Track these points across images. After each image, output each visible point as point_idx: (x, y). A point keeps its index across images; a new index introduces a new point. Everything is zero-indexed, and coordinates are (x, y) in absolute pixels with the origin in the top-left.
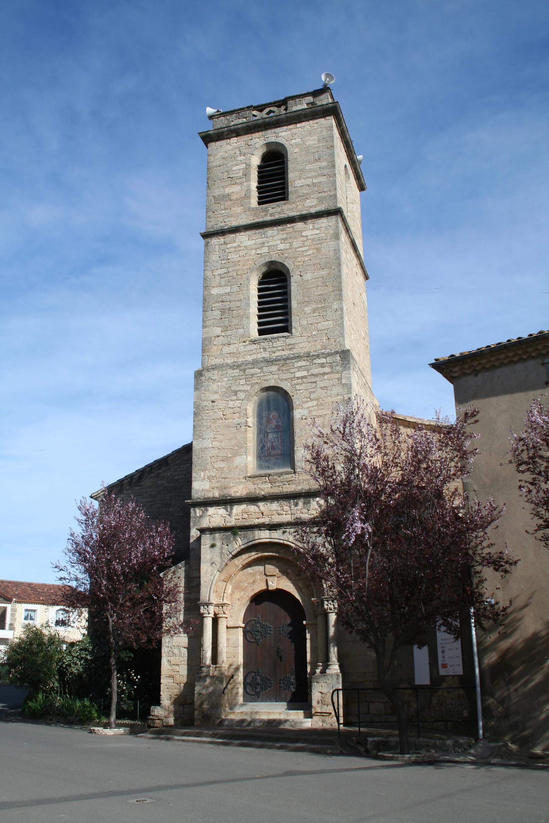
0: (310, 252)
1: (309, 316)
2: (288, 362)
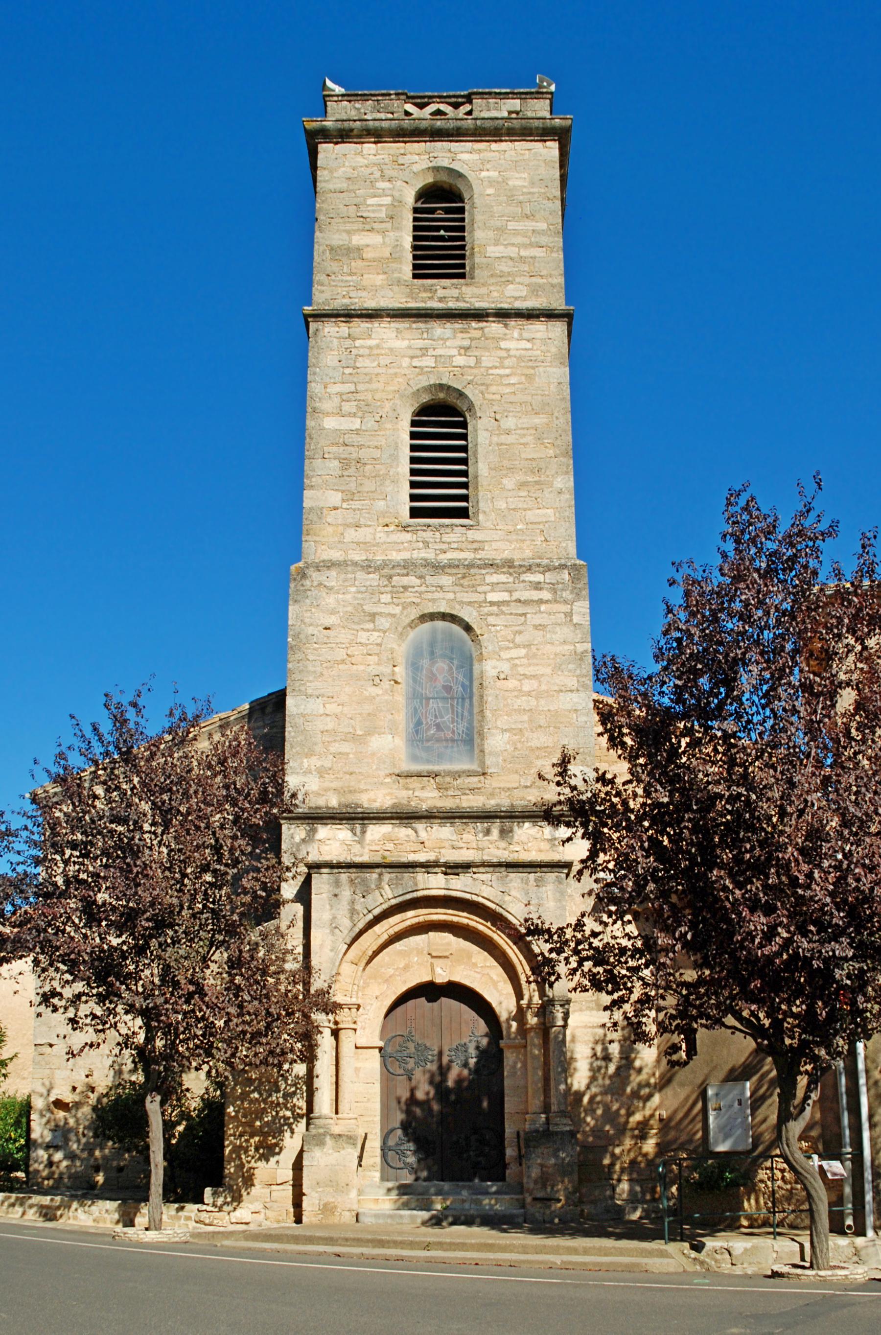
0: (513, 380)
1: (510, 494)
2: (473, 571)
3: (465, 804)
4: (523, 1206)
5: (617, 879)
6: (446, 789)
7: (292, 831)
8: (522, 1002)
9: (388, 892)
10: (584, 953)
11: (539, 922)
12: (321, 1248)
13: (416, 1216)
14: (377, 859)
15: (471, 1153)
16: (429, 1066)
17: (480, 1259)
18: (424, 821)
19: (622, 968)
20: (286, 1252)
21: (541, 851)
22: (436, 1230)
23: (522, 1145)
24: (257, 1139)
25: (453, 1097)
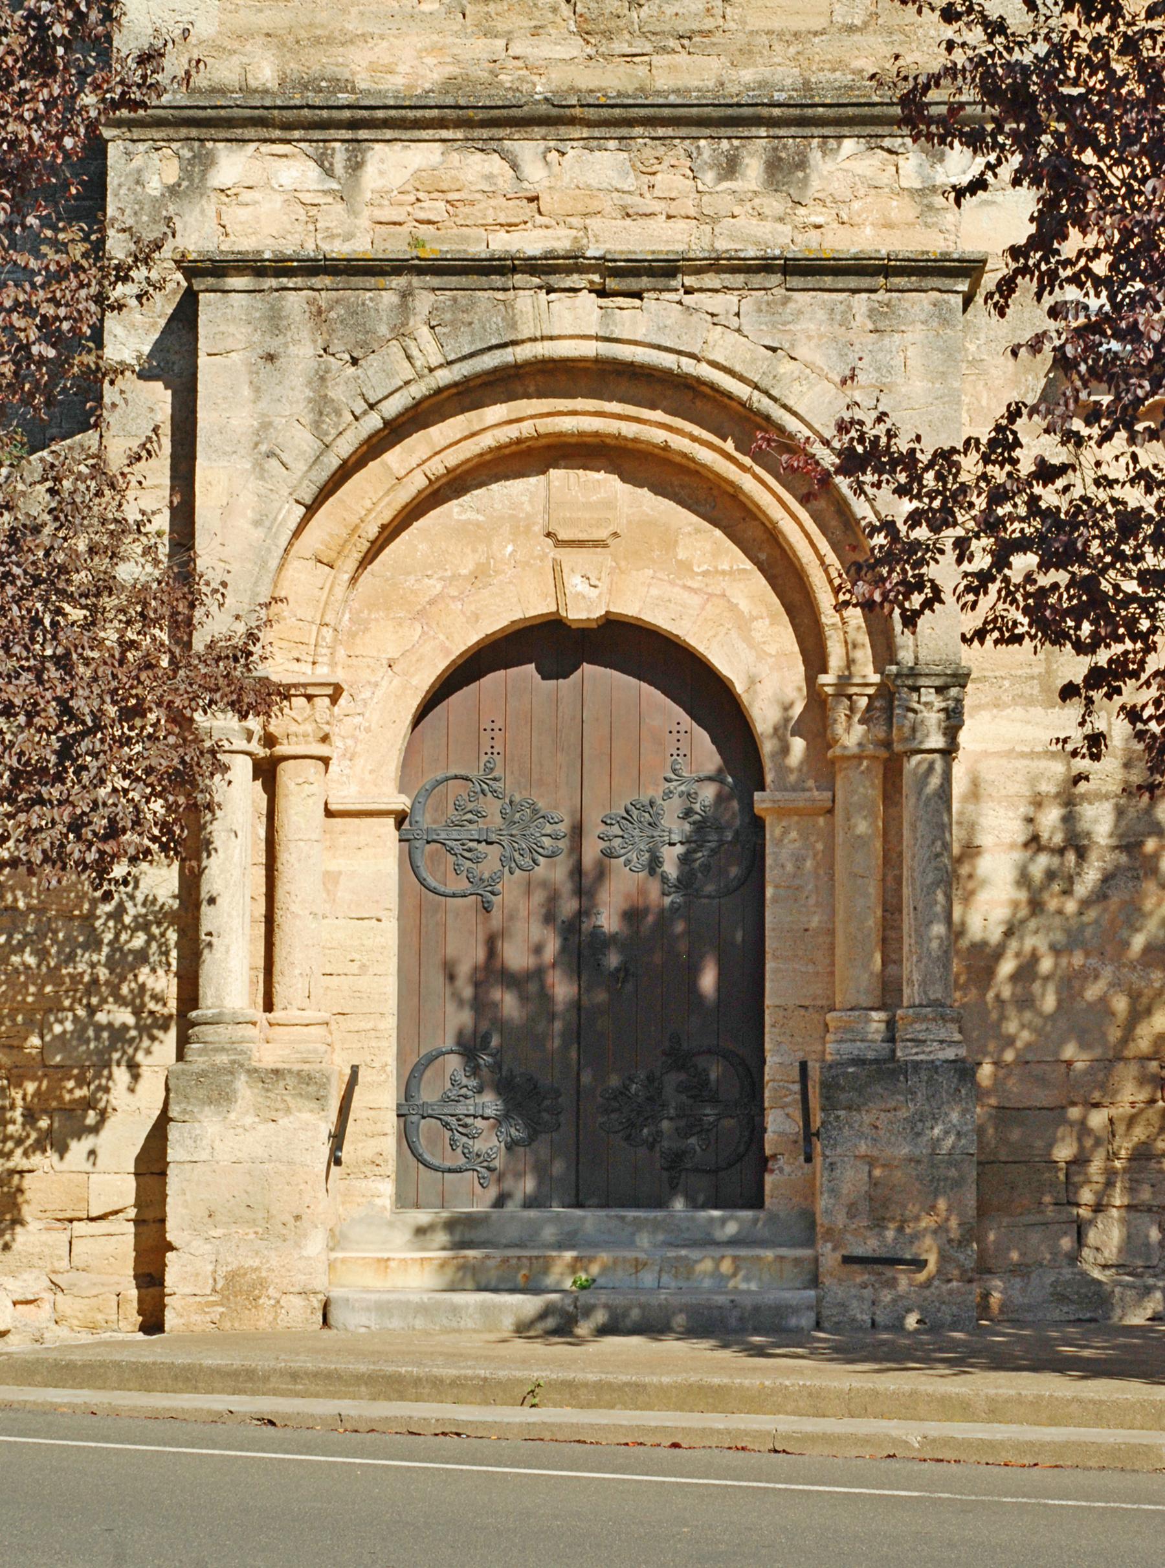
3: (663, 82)
4: (815, 1281)
5: (1117, 307)
6: (608, 35)
7: (138, 162)
8: (823, 679)
9: (428, 349)
10: (1014, 529)
11: (880, 431)
12: (219, 1402)
13: (500, 1308)
14: (396, 247)
15: (665, 1125)
16: (542, 870)
17: (687, 1431)
18: (538, 131)
19: (1126, 574)
20: (115, 1413)
21: (889, 225)
22: (559, 1349)
23: (815, 1102)
24: (31, 1087)
25: (613, 960)
